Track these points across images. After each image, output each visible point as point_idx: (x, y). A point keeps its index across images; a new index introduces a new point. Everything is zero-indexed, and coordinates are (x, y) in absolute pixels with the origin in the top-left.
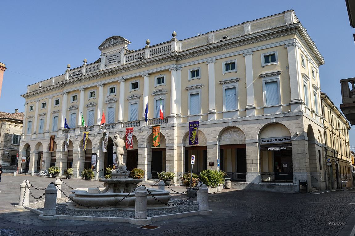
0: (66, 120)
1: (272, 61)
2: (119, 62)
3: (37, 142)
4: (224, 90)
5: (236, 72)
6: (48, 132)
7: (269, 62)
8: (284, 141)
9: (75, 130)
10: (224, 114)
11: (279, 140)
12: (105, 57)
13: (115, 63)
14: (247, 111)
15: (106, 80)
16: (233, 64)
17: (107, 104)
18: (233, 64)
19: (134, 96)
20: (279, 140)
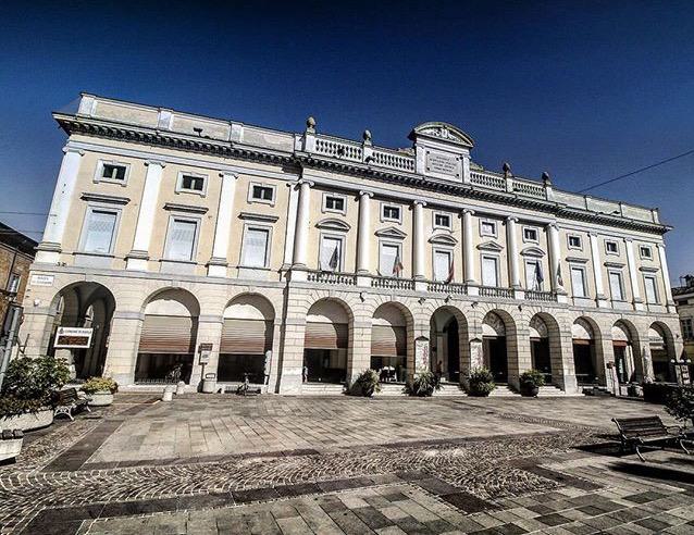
5: (273, 206)
7: (189, 188)
9: (355, 279)
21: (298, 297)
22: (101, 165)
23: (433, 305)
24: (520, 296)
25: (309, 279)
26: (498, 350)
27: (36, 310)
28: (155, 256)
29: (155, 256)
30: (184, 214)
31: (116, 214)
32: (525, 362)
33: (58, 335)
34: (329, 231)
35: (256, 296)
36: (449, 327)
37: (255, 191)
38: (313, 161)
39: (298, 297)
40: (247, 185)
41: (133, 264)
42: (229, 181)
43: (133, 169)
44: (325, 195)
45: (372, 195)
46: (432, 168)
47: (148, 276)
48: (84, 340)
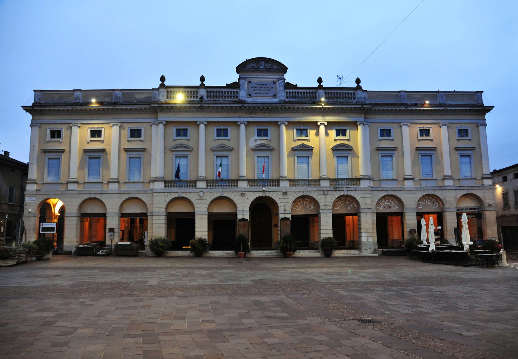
0: (180, 168)
1: (224, 136)
2: (250, 95)
3: (286, 197)
4: (87, 159)
5: (392, 140)
6: (118, 182)
7: (221, 136)
8: (474, 211)
9: (237, 182)
10: (86, 185)
11: (470, 209)
12: (246, 83)
13: (267, 95)
14: (110, 184)
15: (253, 117)
16: (466, 131)
17: (172, 151)
18: (466, 131)
19: (222, 147)
20: (470, 209)
21: (160, 198)
22: (89, 131)
23: (251, 197)
24: (325, 184)
25: (207, 186)
26: (135, 223)
27: (491, 209)
28: (456, 178)
29: (456, 178)
30: (222, 151)
31: (100, 158)
32: (326, 230)
33: (41, 227)
34: (339, 152)
35: (392, 196)
36: (263, 208)
37: (91, 134)
38: (163, 107)
39: (160, 198)
40: (416, 129)
41: (71, 187)
42: (405, 129)
43: (433, 130)
44: (175, 128)
45: (326, 124)
46: (253, 94)
47: (80, 193)
48: (52, 229)
